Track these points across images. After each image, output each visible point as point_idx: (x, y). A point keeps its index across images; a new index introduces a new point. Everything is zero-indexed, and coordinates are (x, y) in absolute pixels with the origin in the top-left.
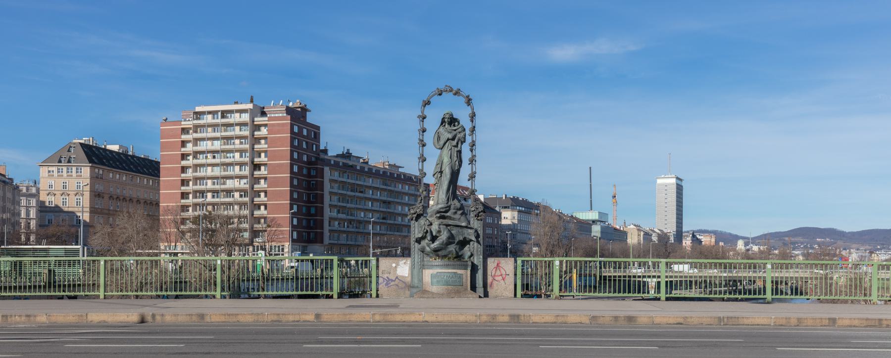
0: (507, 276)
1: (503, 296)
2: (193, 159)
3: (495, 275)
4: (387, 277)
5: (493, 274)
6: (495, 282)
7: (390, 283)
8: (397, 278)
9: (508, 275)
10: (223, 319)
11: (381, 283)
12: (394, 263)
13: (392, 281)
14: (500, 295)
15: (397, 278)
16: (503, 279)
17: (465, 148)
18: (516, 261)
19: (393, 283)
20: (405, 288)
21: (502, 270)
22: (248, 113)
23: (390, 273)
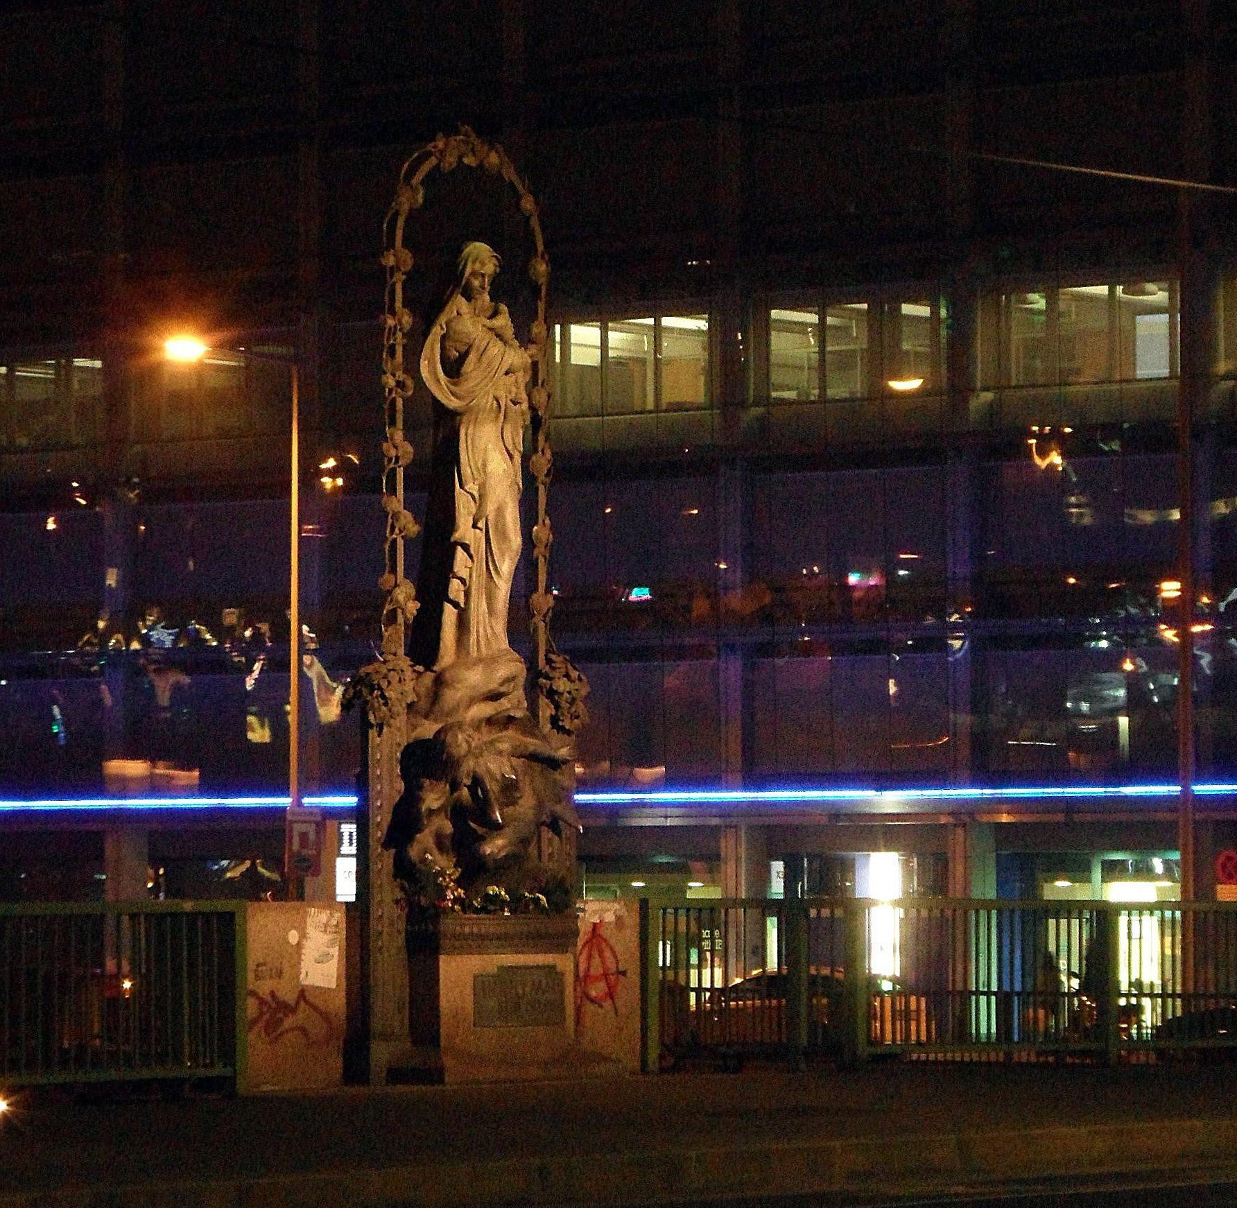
3: (587, 976)
5: (581, 974)
6: (590, 1008)
7: (281, 1020)
9: (624, 973)
13: (289, 1009)
16: (611, 995)
21: (607, 954)
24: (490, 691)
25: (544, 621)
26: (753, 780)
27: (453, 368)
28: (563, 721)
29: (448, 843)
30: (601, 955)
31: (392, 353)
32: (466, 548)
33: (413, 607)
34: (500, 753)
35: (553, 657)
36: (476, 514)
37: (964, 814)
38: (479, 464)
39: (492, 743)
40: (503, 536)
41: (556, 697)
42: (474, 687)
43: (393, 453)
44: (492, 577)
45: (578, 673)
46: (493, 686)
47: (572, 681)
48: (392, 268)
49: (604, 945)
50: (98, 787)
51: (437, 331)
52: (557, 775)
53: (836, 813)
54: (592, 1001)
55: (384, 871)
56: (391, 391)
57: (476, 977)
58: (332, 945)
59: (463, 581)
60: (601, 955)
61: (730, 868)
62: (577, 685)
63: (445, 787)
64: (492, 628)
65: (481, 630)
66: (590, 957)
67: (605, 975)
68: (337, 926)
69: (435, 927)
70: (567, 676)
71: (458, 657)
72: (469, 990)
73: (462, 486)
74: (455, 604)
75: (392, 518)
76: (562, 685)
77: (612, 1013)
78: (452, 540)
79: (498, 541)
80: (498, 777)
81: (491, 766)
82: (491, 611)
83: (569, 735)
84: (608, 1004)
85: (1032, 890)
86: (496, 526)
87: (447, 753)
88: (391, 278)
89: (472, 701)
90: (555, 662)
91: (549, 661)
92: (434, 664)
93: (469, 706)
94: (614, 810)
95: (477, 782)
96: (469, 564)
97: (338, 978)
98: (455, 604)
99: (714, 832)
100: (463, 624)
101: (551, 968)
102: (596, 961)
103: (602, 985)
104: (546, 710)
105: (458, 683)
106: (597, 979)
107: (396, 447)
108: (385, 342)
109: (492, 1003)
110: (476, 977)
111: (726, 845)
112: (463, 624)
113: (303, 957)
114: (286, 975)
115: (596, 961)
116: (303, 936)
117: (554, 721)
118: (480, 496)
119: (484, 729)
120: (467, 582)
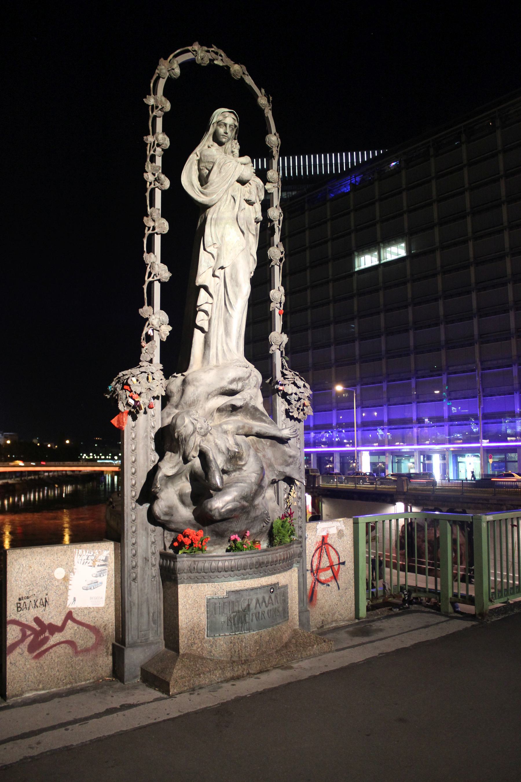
0: (341, 566)
1: (336, 621)
2: (202, 425)
3: (318, 569)
4: (37, 620)
5: (315, 568)
6: (320, 588)
7: (46, 639)
8: (69, 616)
9: (343, 563)
10: (211, 458)
11: (15, 645)
12: (58, 566)
13: (54, 629)
14: (329, 620)
15: (69, 616)
16: (335, 577)
17: (242, 571)
18: (356, 523)
19: (57, 638)
20: (95, 647)
21: (332, 553)
22: (358, 519)
23: (45, 603)
24: (221, 388)
25: (279, 350)
26: (354, 408)
27: (203, 180)
28: (292, 412)
29: (189, 500)
30: (328, 555)
31: (153, 159)
32: (206, 288)
33: (166, 330)
34: (225, 432)
35: (286, 372)
36: (215, 267)
37: (448, 449)
38: (219, 237)
39: (220, 425)
40: (237, 284)
41: (288, 397)
42: (209, 385)
43: (151, 224)
44: (228, 311)
45: (304, 383)
46: (225, 384)
47: (299, 387)
48: (153, 106)
49: (330, 548)
50: (507, 441)
51: (193, 158)
52: (285, 448)
53: (430, 449)
54: (322, 583)
55: (139, 521)
56: (151, 184)
57: (208, 600)
58: (100, 574)
59: (206, 312)
60: (328, 555)
61: (415, 457)
62: (302, 390)
63: (177, 458)
64: (227, 344)
65: (220, 348)
66: (320, 557)
67: (331, 566)
68: (106, 560)
69: (174, 564)
70: (295, 384)
71: (203, 366)
72: (203, 609)
73: (205, 249)
74: (202, 330)
75: (150, 268)
76: (290, 389)
77: (336, 588)
78: (197, 284)
79: (232, 286)
80: (224, 450)
81: (219, 442)
82: (227, 333)
83: (299, 422)
84: (333, 584)
85: (457, 459)
86: (232, 278)
87: (178, 432)
88: (152, 112)
89: (209, 396)
90: (287, 375)
91: (283, 375)
92: (185, 371)
93: (207, 399)
94: (400, 449)
95: (203, 455)
96: (210, 300)
97: (107, 597)
98: (202, 330)
99: (413, 452)
100: (206, 344)
101: (273, 588)
102: (325, 558)
103: (329, 574)
104: (281, 405)
105: (197, 382)
106: (325, 570)
107: (154, 221)
108: (148, 153)
109: (223, 619)
110: (208, 600)
111: (415, 454)
112: (206, 344)
113: (70, 587)
114: (52, 603)
115: (325, 558)
116: (71, 570)
117: (287, 412)
118: (218, 255)
119: (216, 415)
120: (210, 313)
